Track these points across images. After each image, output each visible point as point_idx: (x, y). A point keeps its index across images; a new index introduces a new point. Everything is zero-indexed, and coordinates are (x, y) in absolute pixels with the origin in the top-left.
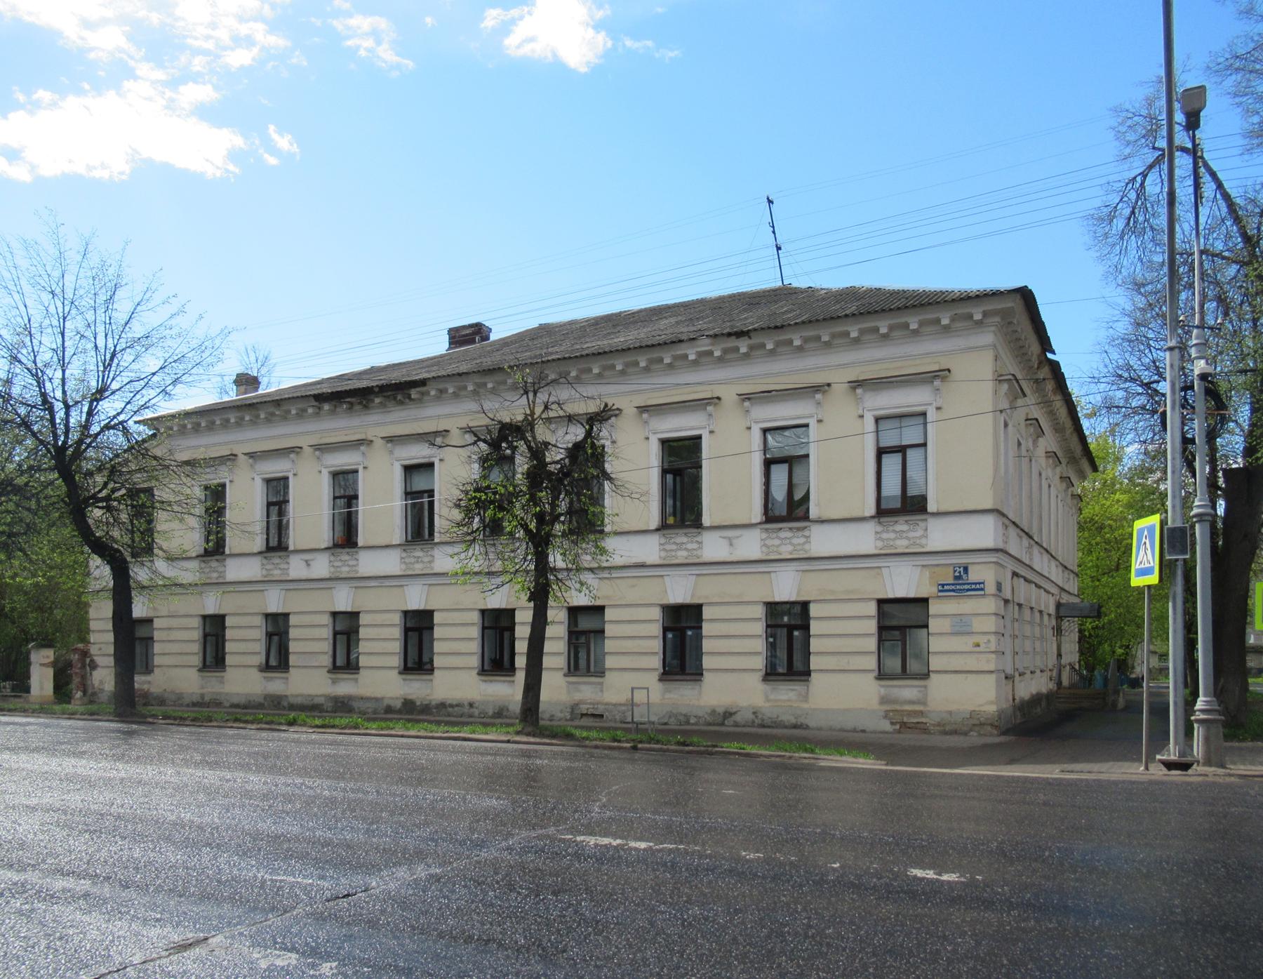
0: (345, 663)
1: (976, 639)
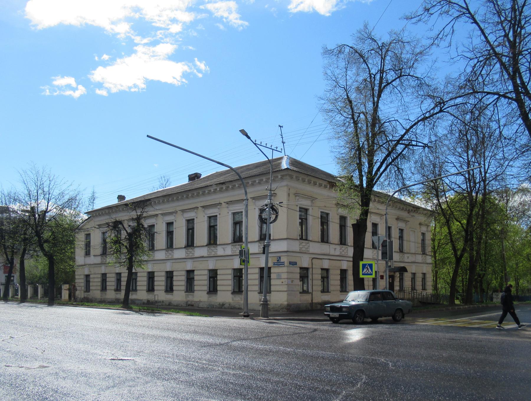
0: (213, 289)
1: (282, 280)
